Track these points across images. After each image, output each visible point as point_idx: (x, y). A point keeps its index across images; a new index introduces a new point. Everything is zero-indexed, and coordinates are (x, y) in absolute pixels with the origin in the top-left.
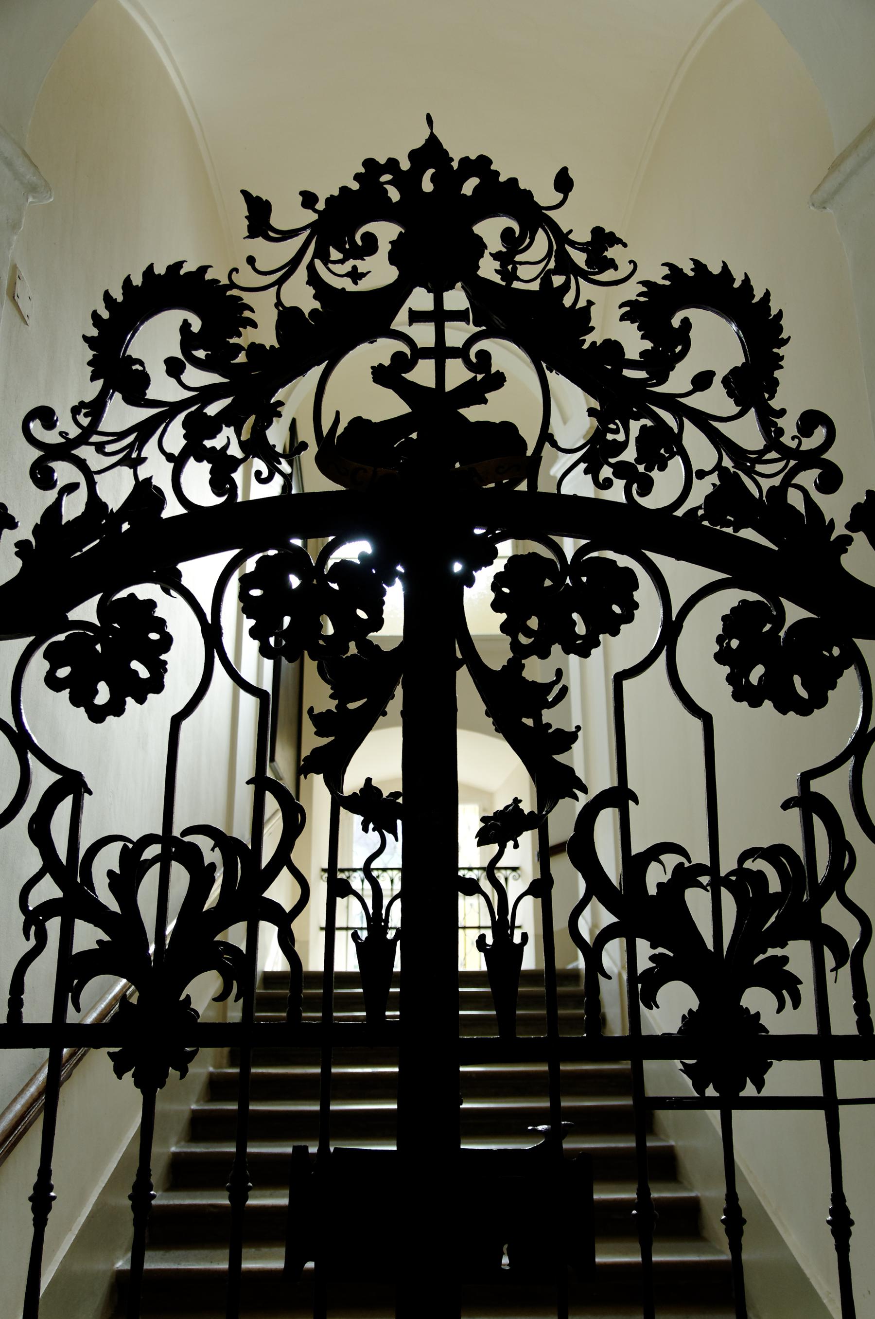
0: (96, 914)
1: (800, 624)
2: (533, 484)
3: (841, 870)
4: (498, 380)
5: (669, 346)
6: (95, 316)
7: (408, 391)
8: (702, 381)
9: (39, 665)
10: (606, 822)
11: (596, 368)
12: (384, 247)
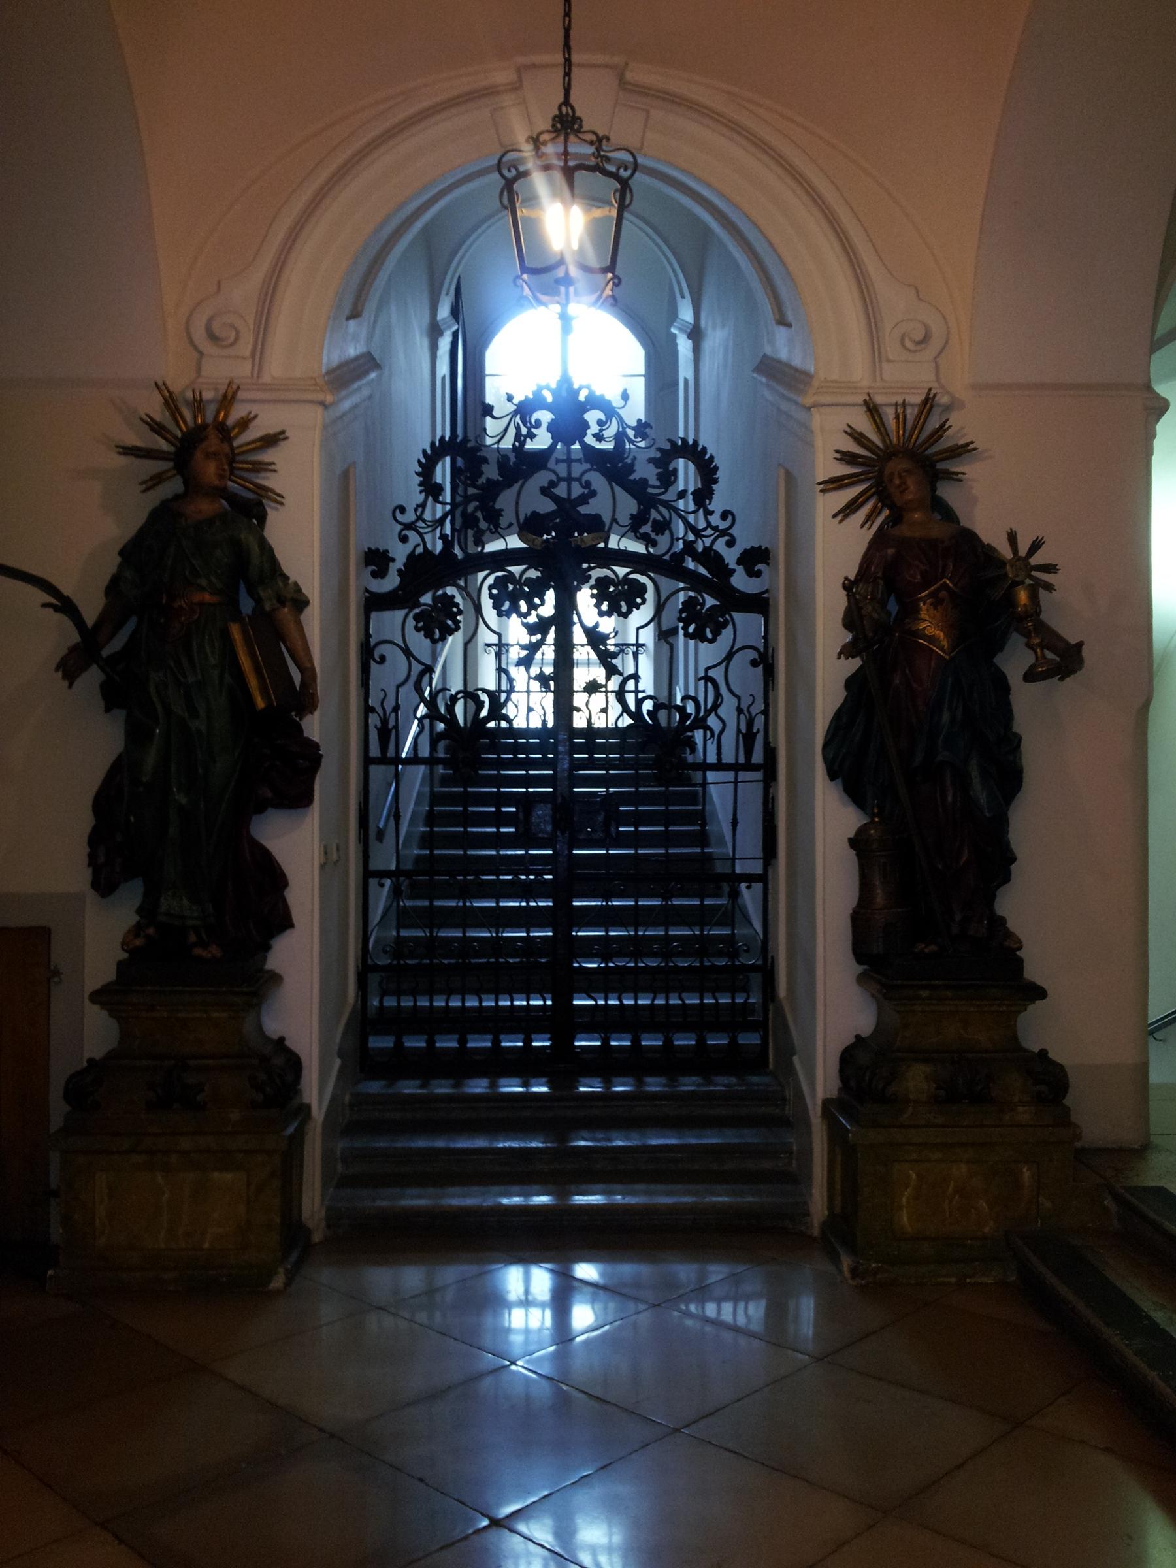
0: (442, 719)
1: (712, 607)
2: (606, 544)
3: (715, 707)
4: (593, 494)
5: (668, 478)
6: (419, 461)
7: (556, 499)
8: (682, 495)
9: (411, 622)
10: (631, 685)
11: (638, 490)
12: (544, 425)
